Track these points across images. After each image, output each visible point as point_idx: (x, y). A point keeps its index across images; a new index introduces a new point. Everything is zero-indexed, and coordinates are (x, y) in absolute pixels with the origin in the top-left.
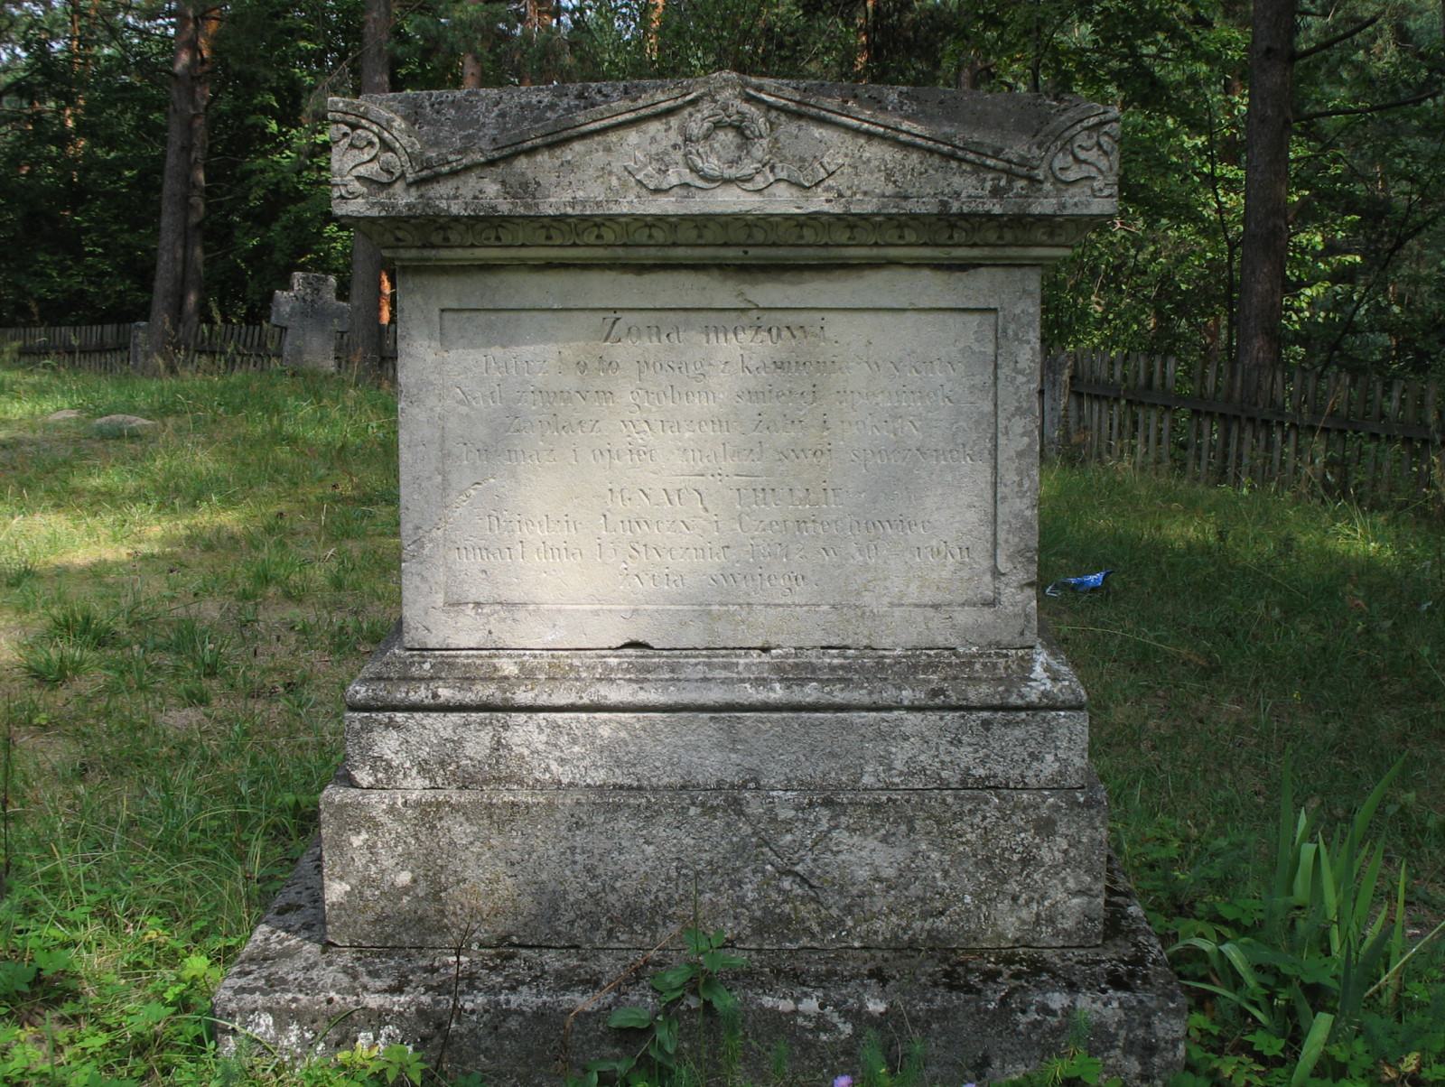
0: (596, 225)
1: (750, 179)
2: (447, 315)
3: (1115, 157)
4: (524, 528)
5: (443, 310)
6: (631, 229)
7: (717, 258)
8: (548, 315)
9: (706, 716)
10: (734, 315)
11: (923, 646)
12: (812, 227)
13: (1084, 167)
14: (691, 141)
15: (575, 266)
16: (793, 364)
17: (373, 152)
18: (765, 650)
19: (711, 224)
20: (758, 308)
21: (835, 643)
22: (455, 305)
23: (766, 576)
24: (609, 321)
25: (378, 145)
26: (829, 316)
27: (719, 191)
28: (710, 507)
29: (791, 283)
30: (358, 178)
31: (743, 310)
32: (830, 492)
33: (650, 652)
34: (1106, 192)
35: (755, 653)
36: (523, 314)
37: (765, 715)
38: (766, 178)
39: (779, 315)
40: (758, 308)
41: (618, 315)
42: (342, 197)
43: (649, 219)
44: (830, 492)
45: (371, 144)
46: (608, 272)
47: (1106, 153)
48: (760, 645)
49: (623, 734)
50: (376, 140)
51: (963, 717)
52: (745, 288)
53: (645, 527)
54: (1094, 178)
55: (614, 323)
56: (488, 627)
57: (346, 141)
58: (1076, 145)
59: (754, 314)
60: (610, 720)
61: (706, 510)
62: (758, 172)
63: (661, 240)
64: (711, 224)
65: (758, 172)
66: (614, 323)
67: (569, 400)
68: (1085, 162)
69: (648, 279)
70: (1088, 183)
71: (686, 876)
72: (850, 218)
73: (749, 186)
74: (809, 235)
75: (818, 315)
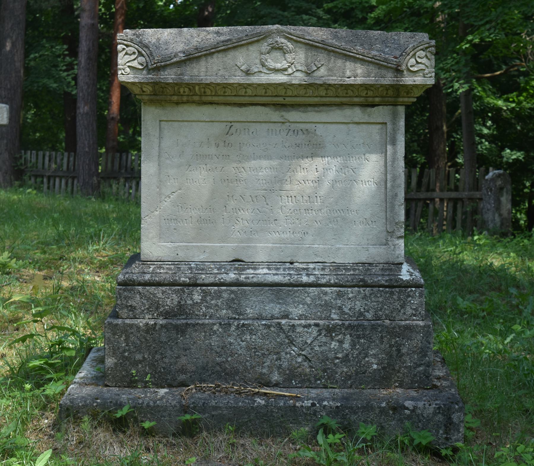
0: (224, 87)
1: (285, 70)
2: (163, 123)
3: (433, 62)
4: (193, 211)
5: (160, 121)
6: (238, 89)
7: (273, 101)
8: (204, 123)
9: (267, 288)
10: (280, 124)
11: (357, 262)
12: (372, 90)
13: (420, 65)
14: (263, 54)
15: (215, 103)
16: (304, 145)
17: (136, 56)
18: (292, 263)
19: (270, 88)
20: (289, 122)
21: (320, 261)
22: (165, 119)
23: (291, 232)
24: (228, 127)
25: (137, 53)
26: (318, 125)
27: (273, 74)
28: (269, 203)
29: (303, 112)
30: (129, 67)
31: (283, 123)
32: (319, 198)
33: (244, 263)
34: (429, 75)
35: (288, 264)
36: (194, 123)
37: (291, 288)
38: (292, 69)
39: (298, 125)
40: (289, 122)
41: (232, 124)
42: (122, 74)
43: (387, 86)
44: (319, 198)
45: (134, 53)
46: (228, 106)
47: (429, 59)
48: (289, 261)
49: (232, 296)
50: (136, 51)
51: (372, 290)
52: (284, 113)
53: (242, 211)
54: (424, 70)
55: (230, 127)
56: (176, 252)
57: (124, 52)
58: (417, 56)
59: (288, 124)
60: (228, 290)
61: (267, 204)
62: (289, 67)
63: (250, 94)
64: (414, 89)
65: (289, 67)
66: (230, 127)
67: (212, 158)
68: (421, 63)
69: (244, 109)
70: (422, 71)
71: (258, 355)
72: (326, 86)
73: (286, 73)
74: (310, 92)
75: (314, 125)
